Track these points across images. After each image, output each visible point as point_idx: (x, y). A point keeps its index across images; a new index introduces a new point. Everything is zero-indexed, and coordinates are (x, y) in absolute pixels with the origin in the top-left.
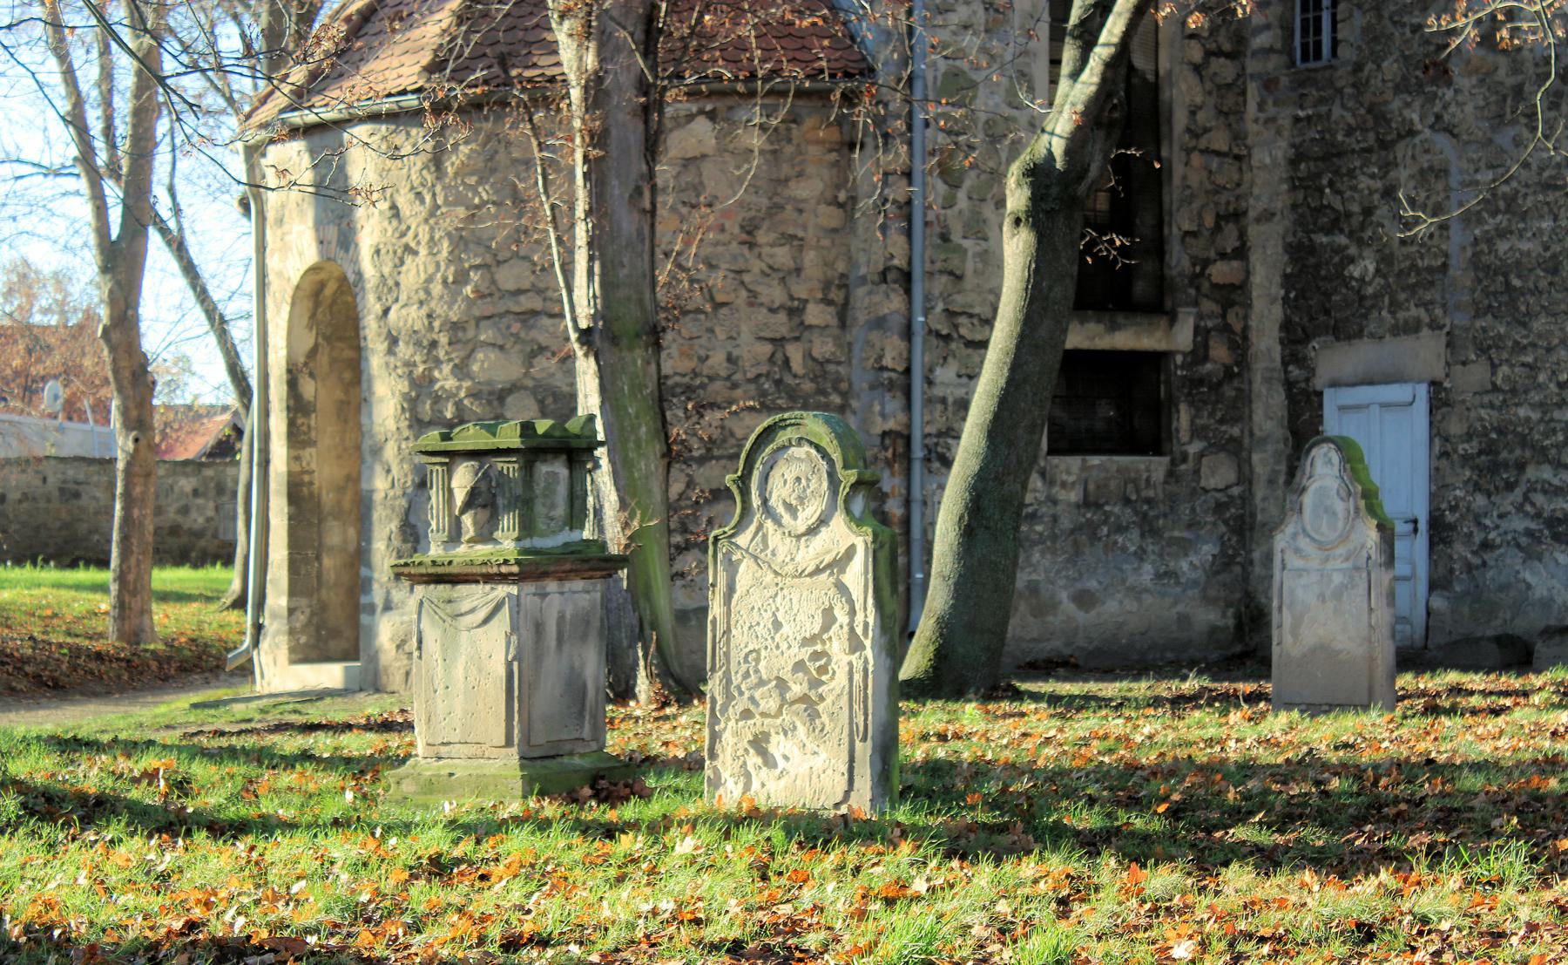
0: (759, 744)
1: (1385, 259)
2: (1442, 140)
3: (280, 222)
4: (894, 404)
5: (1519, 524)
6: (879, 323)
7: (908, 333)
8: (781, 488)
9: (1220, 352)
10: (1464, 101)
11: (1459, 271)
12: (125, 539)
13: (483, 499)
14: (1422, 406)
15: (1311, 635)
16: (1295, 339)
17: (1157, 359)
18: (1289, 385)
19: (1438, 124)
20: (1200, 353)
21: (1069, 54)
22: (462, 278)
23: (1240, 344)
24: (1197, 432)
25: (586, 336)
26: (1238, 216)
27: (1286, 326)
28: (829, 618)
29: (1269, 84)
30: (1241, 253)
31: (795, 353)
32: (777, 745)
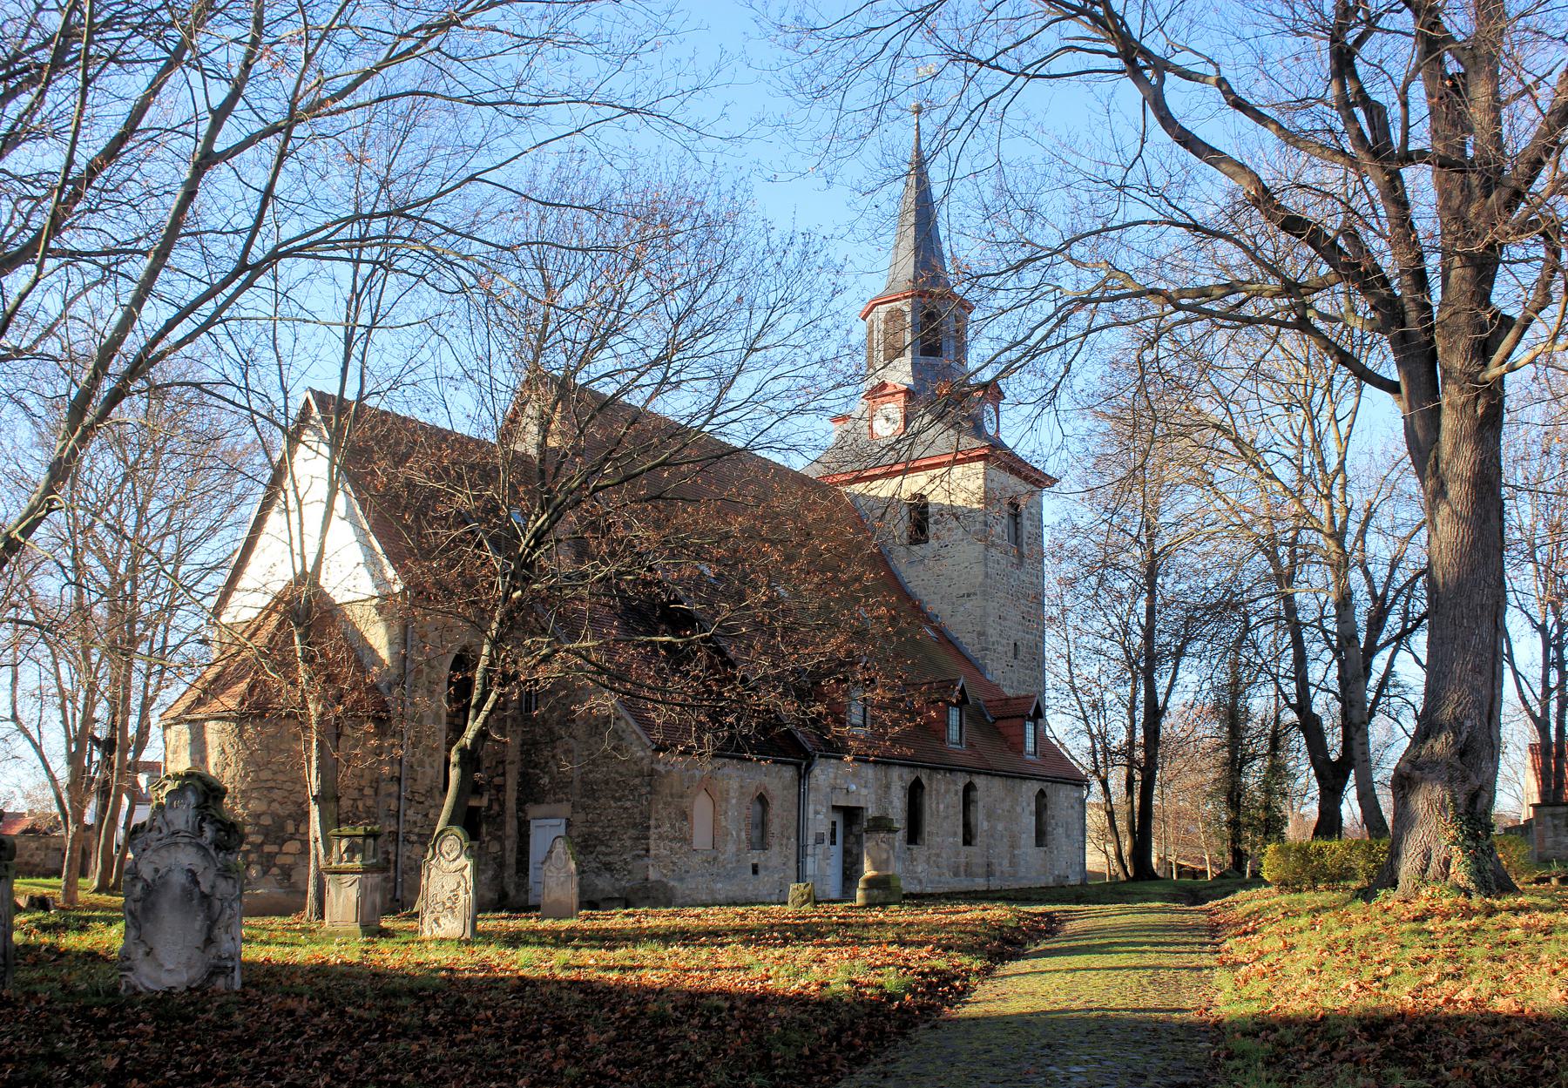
0: (436, 920)
1: (552, 779)
2: (572, 741)
3: (175, 752)
4: (393, 822)
5: (594, 865)
6: (390, 795)
7: (399, 798)
8: (445, 848)
9: (496, 807)
10: (580, 730)
11: (577, 783)
12: (69, 865)
13: (351, 850)
14: (563, 826)
15: (553, 896)
16: (521, 803)
17: (479, 808)
18: (519, 818)
19: (571, 735)
20: (490, 807)
21: (472, 713)
22: (247, 775)
23: (502, 805)
24: (488, 834)
25: (315, 798)
26: (503, 762)
27: (518, 799)
28: (459, 885)
29: (514, 719)
30: (504, 774)
31: (360, 804)
32: (442, 921)
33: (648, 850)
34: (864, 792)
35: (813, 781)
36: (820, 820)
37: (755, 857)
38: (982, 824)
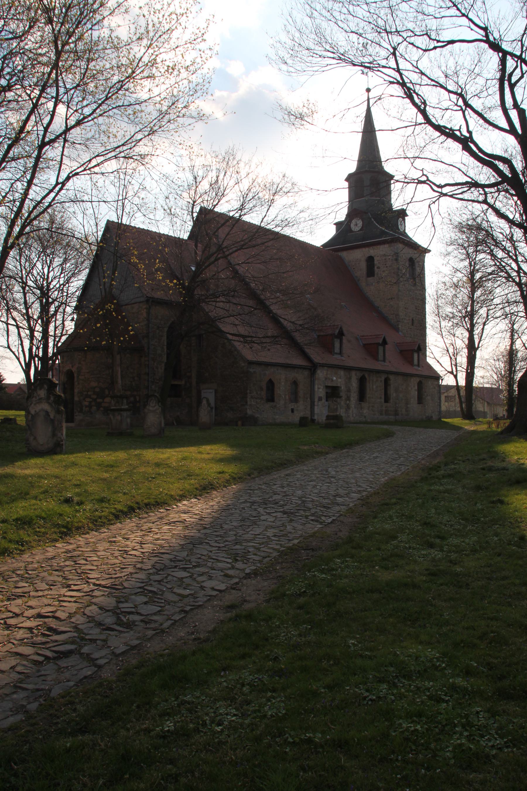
14: (214, 393)
33: (247, 402)
34: (339, 380)
35: (317, 376)
36: (320, 391)
37: (292, 406)
38: (393, 394)
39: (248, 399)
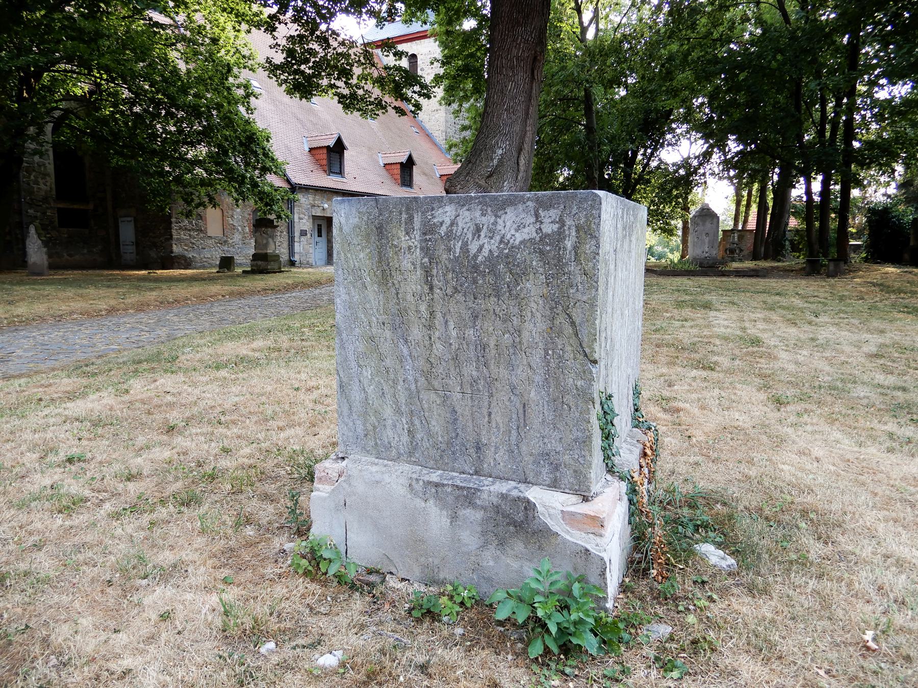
33: (171, 236)
39: (174, 232)
